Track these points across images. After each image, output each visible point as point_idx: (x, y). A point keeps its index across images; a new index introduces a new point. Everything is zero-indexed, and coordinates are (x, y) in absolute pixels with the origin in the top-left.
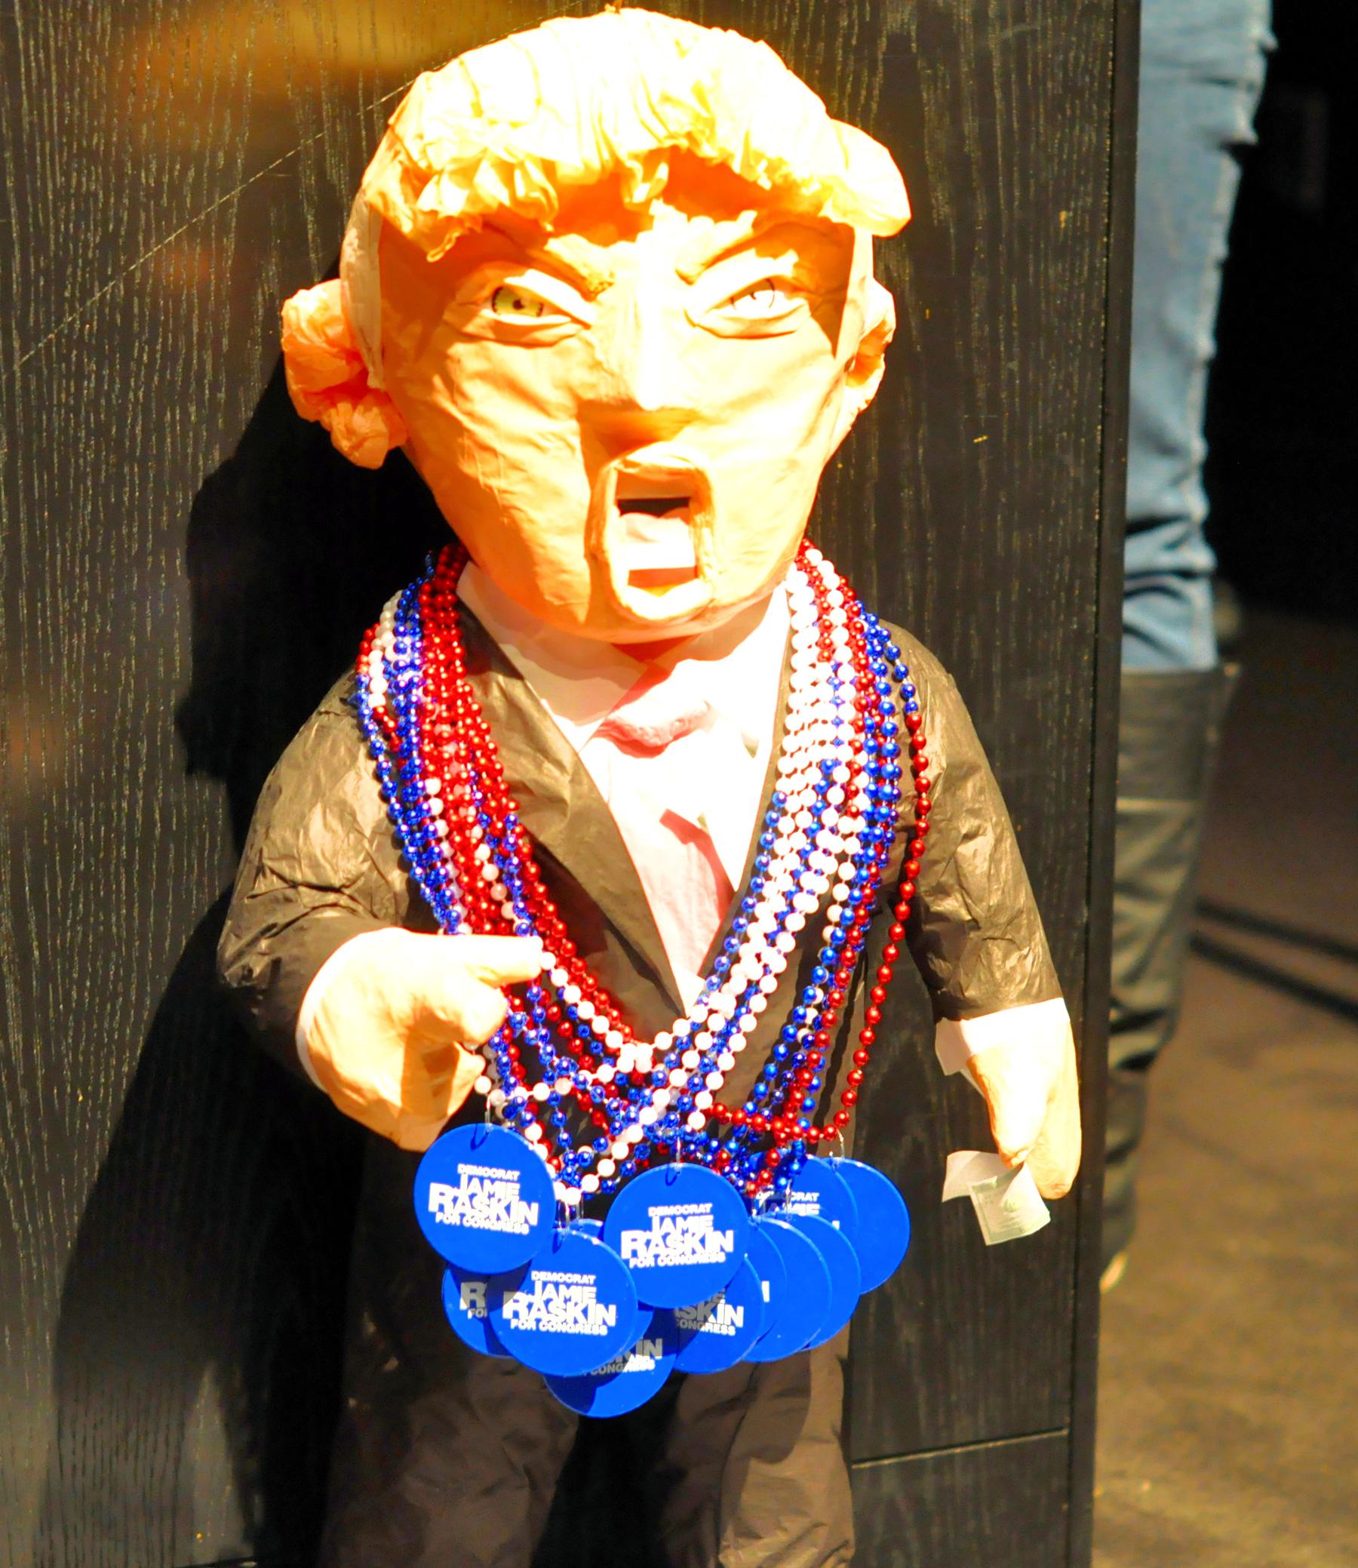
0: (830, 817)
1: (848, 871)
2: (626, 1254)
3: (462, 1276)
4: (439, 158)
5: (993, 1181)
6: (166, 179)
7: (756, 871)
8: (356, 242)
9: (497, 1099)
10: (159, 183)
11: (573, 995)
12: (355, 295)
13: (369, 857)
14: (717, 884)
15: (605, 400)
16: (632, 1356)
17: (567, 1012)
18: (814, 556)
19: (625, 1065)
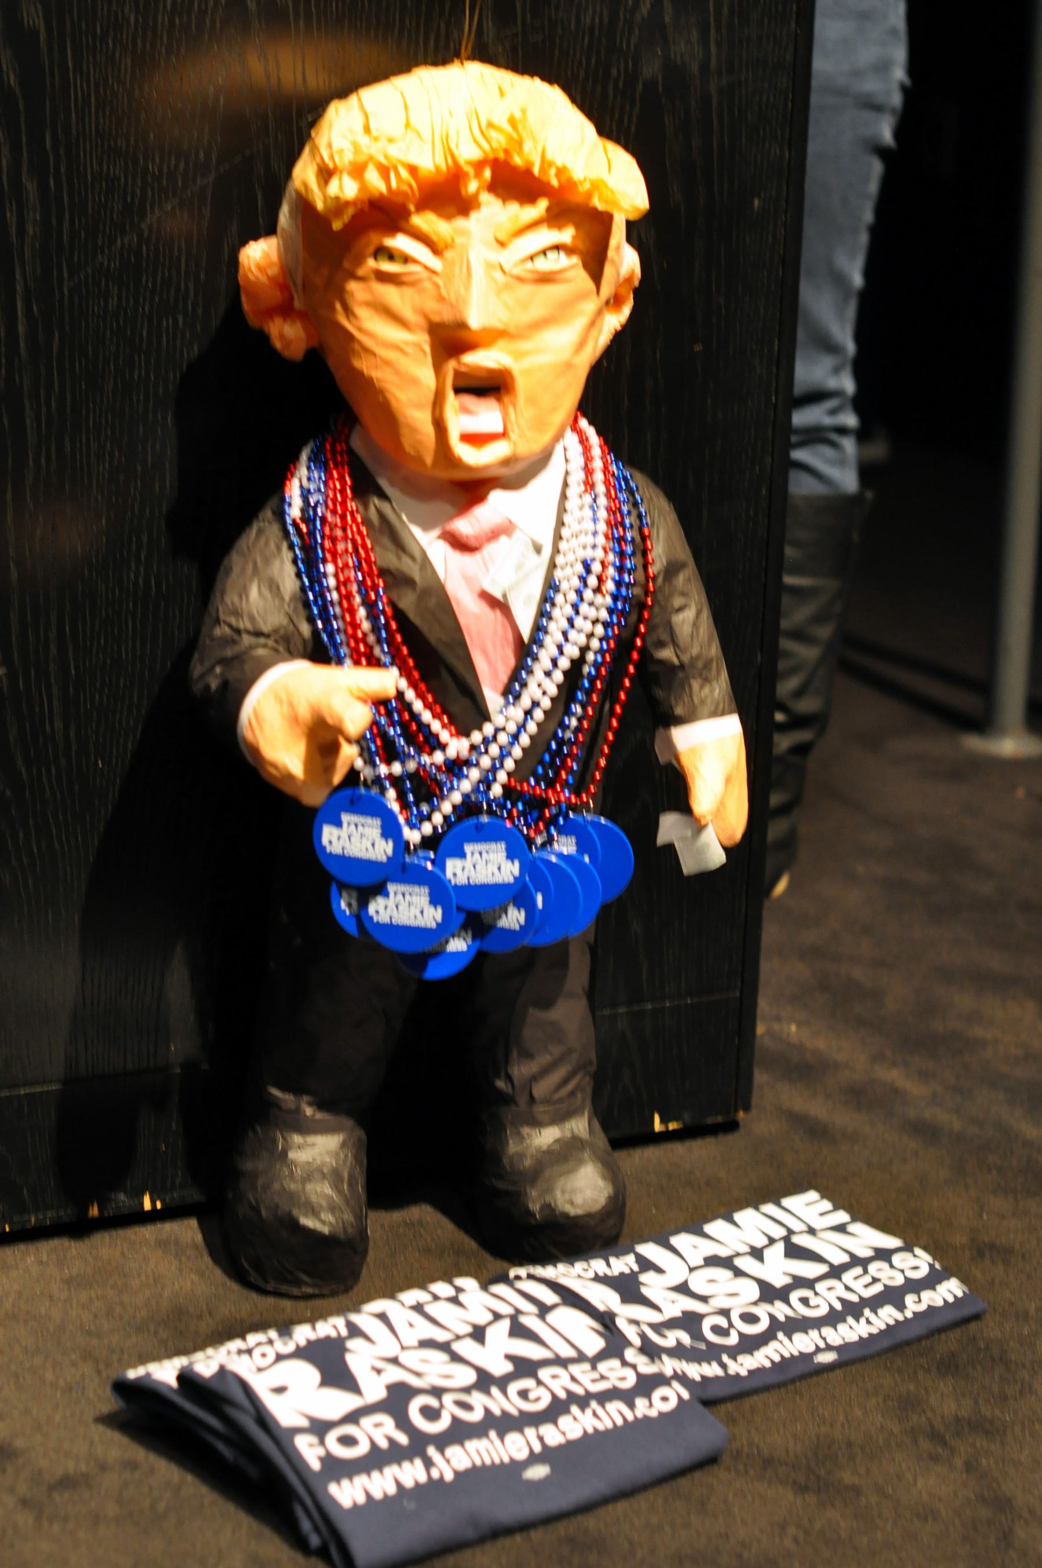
0: (588, 594)
1: (600, 630)
2: (449, 874)
3: (343, 886)
4: (345, 158)
5: (689, 833)
6: (165, 170)
7: (539, 629)
8: (287, 215)
9: (366, 773)
10: (161, 171)
11: (418, 706)
12: (286, 249)
13: (287, 614)
14: (513, 635)
15: (447, 323)
16: (451, 940)
17: (415, 717)
18: (583, 423)
19: (452, 752)
